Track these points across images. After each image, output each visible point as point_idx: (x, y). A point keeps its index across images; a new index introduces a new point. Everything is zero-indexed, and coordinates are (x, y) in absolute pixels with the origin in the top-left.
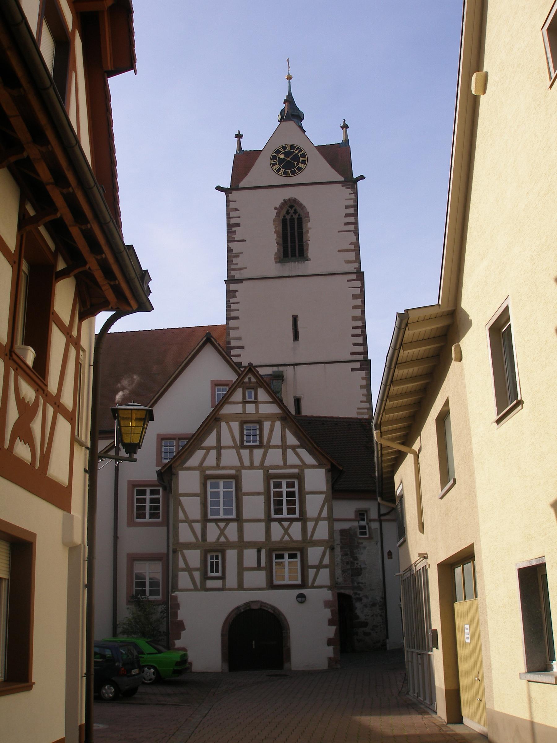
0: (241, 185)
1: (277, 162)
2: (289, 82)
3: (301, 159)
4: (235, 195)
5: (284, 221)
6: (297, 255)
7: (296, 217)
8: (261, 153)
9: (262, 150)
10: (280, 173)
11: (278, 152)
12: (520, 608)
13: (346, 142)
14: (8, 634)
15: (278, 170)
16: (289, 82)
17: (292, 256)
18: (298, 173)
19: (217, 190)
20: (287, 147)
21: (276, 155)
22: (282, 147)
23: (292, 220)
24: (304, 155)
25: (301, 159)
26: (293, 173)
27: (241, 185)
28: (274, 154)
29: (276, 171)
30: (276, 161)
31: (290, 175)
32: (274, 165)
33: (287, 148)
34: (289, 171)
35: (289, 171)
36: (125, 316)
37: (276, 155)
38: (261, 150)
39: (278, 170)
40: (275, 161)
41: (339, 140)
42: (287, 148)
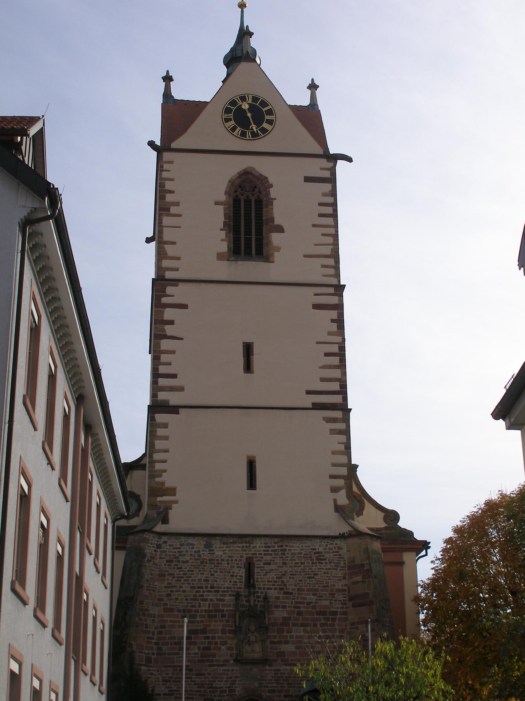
0: (174, 145)
1: (232, 117)
2: (242, 12)
3: (267, 117)
4: (167, 156)
5: (236, 202)
6: (254, 252)
7: (253, 199)
8: (207, 105)
9: (210, 101)
10: (235, 133)
11: (243, 98)
12: (24, 410)
13: (313, 104)
14: (80, 486)
15: (233, 129)
16: (242, 12)
17: (257, 254)
18: (261, 135)
19: (308, 89)
20: (247, 98)
21: (231, 107)
22: (239, 97)
23: (248, 202)
24: (270, 112)
25: (267, 117)
26: (255, 135)
27: (174, 145)
28: (227, 105)
29: (230, 129)
30: (231, 115)
31: (250, 138)
32: (227, 120)
33: (247, 100)
34: (249, 132)
35: (249, 132)
36: (151, 243)
37: (231, 107)
38: (209, 101)
39: (233, 129)
40: (228, 115)
41: (306, 102)
42: (247, 100)
